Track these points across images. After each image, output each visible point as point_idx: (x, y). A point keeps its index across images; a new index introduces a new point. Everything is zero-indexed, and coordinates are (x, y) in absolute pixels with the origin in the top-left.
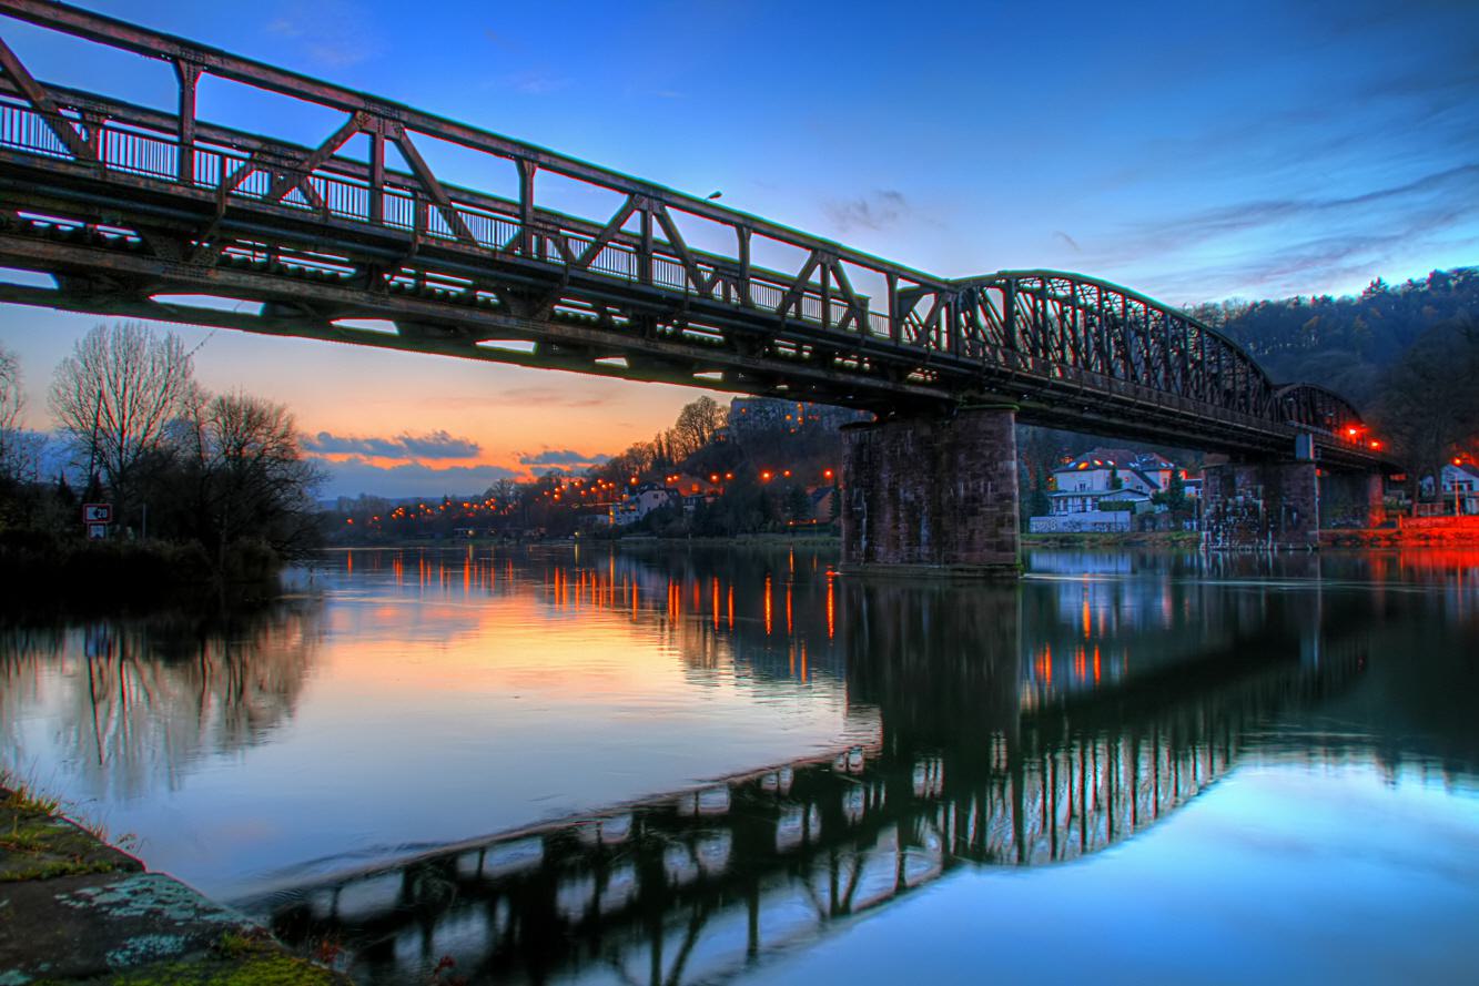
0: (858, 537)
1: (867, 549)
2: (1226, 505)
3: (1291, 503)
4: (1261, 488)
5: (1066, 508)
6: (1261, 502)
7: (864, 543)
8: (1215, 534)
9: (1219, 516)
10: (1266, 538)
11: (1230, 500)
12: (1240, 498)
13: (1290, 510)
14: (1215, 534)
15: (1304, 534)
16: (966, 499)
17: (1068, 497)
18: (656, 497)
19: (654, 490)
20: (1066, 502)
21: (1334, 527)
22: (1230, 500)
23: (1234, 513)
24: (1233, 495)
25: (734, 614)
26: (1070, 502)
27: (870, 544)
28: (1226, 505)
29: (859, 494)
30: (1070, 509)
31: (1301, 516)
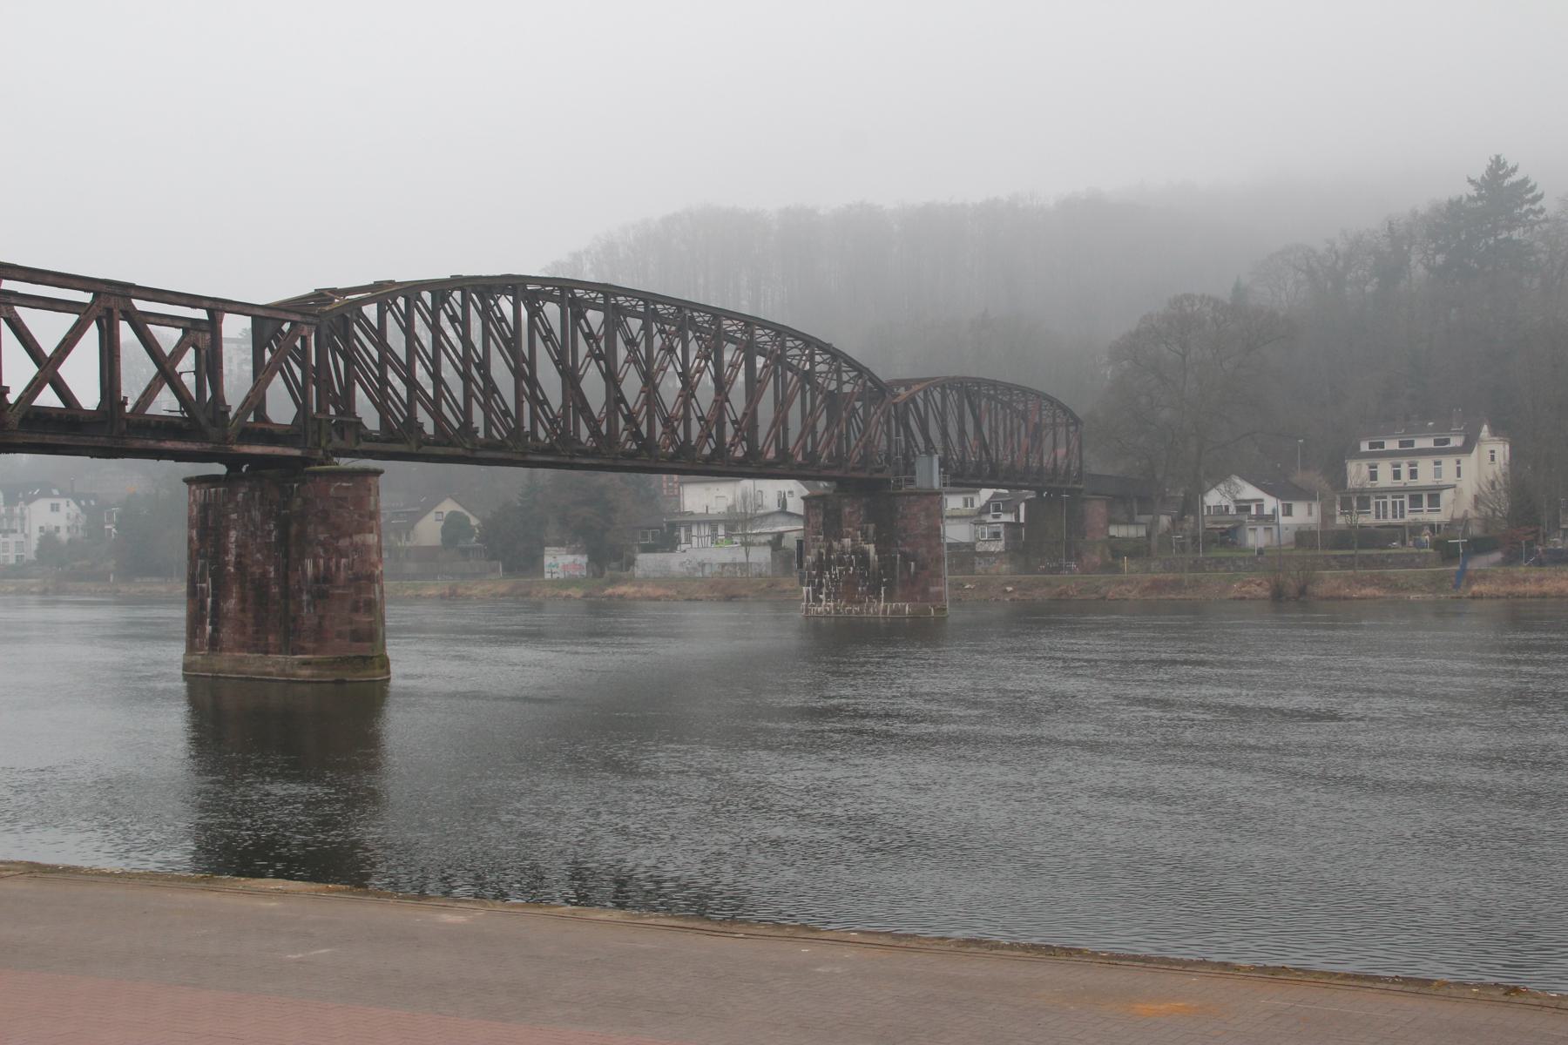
0: (202, 622)
1: (212, 636)
2: (830, 550)
3: (907, 549)
4: (872, 527)
5: (689, 541)
6: (871, 548)
7: (209, 628)
8: (817, 591)
9: (822, 565)
10: (878, 598)
11: (835, 544)
12: (847, 541)
13: (906, 558)
14: (817, 591)
15: (925, 591)
16: (316, 579)
17: (692, 523)
18: (55, 508)
19: (52, 496)
20: (689, 530)
21: (1044, 572)
22: (835, 544)
23: (840, 562)
24: (839, 537)
25: (1350, 548)
26: (694, 531)
27: (215, 630)
28: (830, 550)
29: (203, 566)
30: (694, 540)
31: (922, 567)
